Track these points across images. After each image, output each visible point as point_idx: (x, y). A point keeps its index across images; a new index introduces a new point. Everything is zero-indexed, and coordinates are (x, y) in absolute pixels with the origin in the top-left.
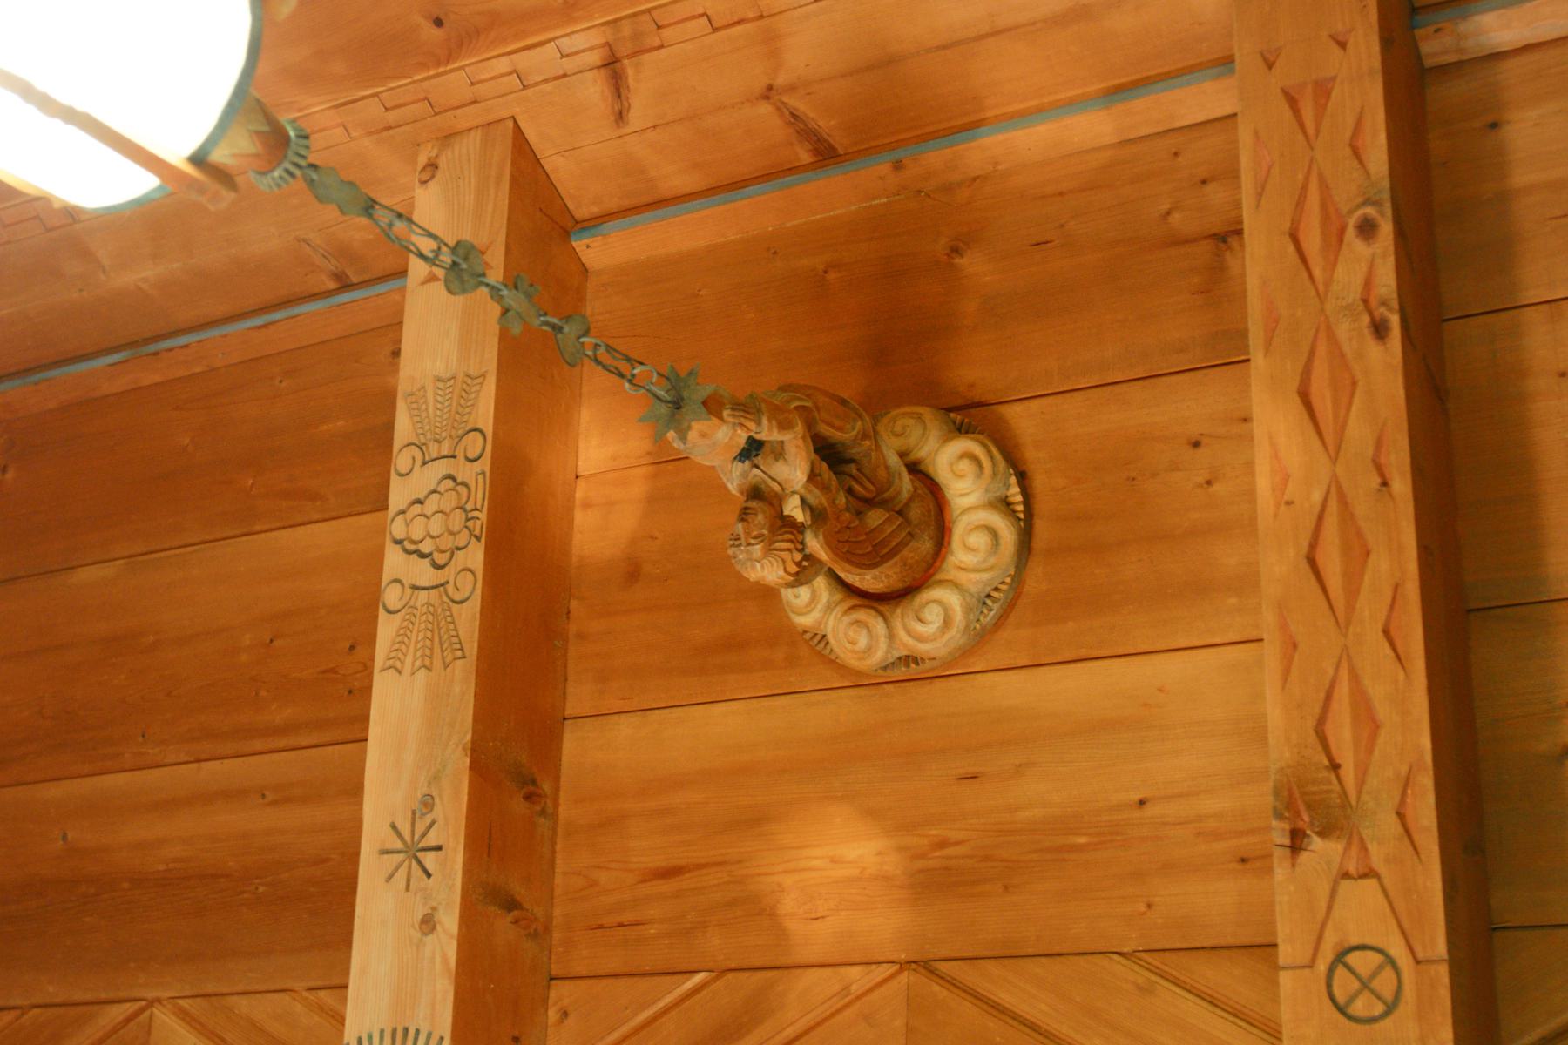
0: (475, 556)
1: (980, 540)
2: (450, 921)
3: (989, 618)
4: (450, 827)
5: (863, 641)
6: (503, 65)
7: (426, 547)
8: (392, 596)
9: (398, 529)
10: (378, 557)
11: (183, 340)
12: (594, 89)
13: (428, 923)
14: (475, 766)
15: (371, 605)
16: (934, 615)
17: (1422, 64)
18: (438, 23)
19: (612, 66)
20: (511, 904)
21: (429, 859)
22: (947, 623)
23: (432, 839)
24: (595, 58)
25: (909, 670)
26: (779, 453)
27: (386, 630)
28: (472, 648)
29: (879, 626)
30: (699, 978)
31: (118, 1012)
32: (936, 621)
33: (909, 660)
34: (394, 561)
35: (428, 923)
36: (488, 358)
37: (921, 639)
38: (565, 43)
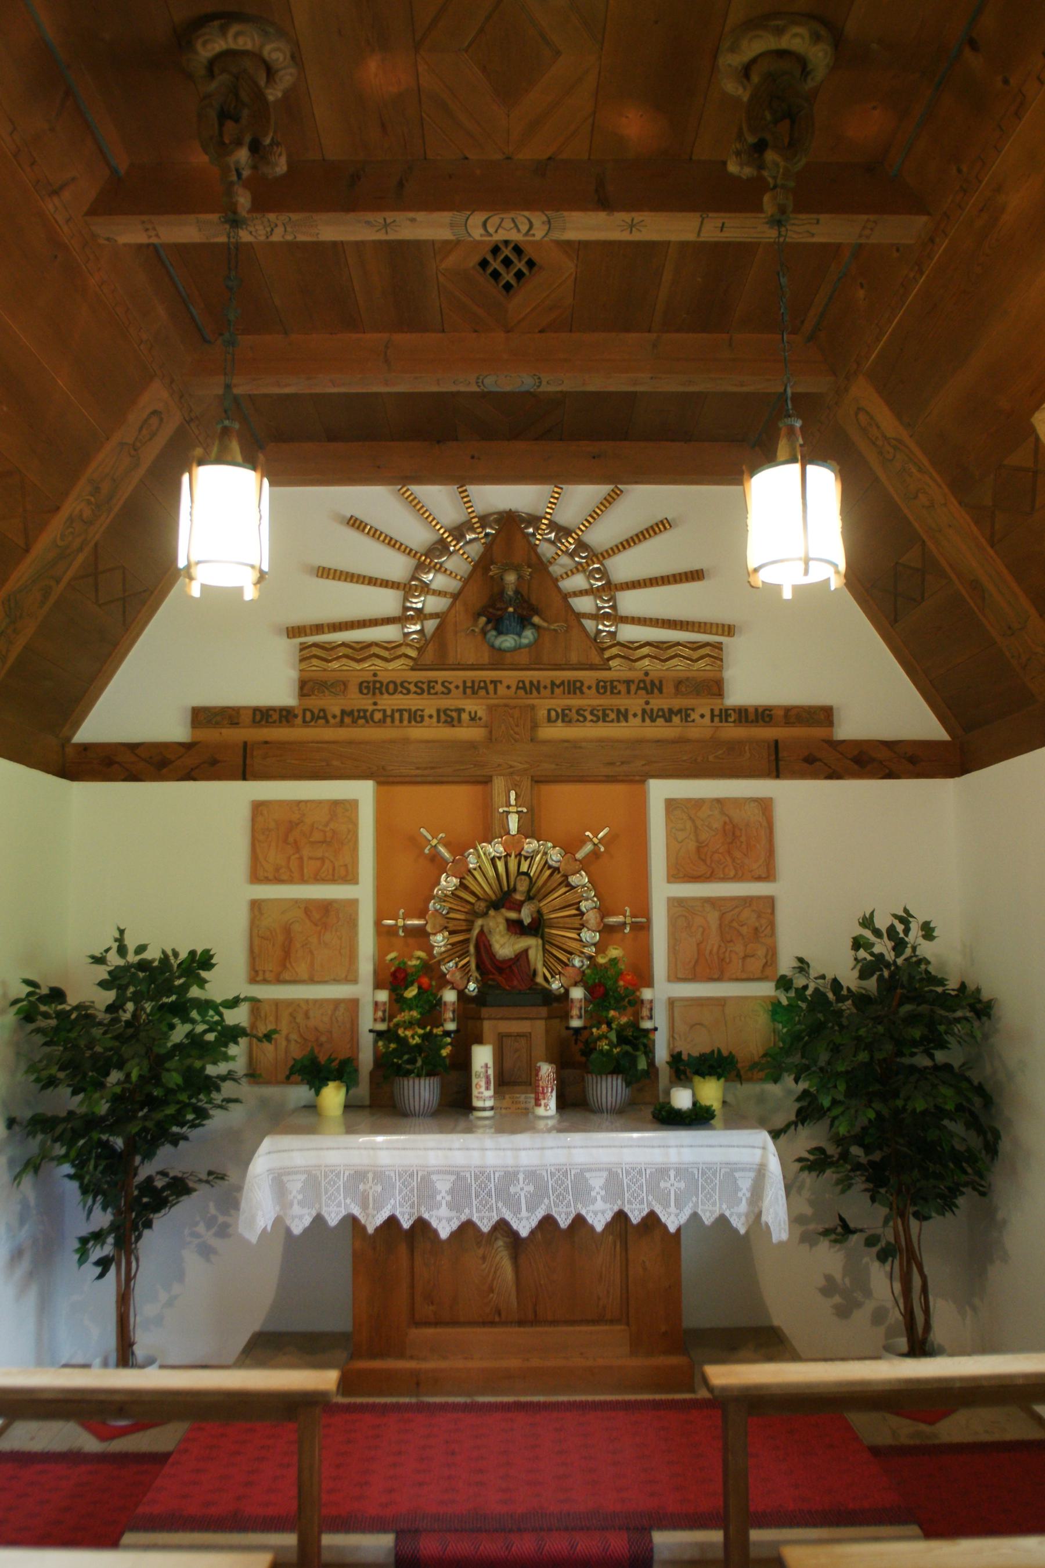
0: (272, 216)
1: (241, 41)
2: (411, 215)
3: (271, 30)
4: (378, 217)
5: (288, 77)
6: (65, 229)
7: (269, 229)
8: (289, 238)
9: (262, 238)
10: (271, 243)
11: (181, 289)
12: (66, 195)
13: (413, 220)
14: (353, 211)
15: (293, 246)
16: (275, 56)
17: (787, 1071)
18: (56, 257)
19: (55, 193)
20: (401, 185)
21: (388, 221)
22: (278, 49)
23: (382, 221)
24: (56, 199)
25: (296, 58)
26: (237, 162)
27: (301, 238)
28: (307, 214)
29: (281, 73)
30: (424, 115)
31: (441, 279)
32: (276, 52)
33: (293, 57)
34: (276, 237)
35: (413, 220)
36: (192, 218)
37: (285, 59)
38: (52, 210)
